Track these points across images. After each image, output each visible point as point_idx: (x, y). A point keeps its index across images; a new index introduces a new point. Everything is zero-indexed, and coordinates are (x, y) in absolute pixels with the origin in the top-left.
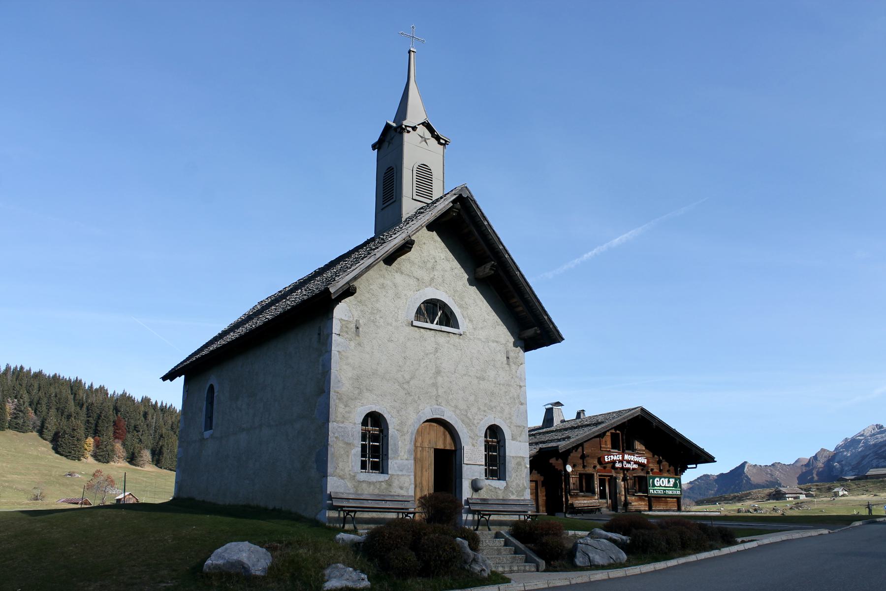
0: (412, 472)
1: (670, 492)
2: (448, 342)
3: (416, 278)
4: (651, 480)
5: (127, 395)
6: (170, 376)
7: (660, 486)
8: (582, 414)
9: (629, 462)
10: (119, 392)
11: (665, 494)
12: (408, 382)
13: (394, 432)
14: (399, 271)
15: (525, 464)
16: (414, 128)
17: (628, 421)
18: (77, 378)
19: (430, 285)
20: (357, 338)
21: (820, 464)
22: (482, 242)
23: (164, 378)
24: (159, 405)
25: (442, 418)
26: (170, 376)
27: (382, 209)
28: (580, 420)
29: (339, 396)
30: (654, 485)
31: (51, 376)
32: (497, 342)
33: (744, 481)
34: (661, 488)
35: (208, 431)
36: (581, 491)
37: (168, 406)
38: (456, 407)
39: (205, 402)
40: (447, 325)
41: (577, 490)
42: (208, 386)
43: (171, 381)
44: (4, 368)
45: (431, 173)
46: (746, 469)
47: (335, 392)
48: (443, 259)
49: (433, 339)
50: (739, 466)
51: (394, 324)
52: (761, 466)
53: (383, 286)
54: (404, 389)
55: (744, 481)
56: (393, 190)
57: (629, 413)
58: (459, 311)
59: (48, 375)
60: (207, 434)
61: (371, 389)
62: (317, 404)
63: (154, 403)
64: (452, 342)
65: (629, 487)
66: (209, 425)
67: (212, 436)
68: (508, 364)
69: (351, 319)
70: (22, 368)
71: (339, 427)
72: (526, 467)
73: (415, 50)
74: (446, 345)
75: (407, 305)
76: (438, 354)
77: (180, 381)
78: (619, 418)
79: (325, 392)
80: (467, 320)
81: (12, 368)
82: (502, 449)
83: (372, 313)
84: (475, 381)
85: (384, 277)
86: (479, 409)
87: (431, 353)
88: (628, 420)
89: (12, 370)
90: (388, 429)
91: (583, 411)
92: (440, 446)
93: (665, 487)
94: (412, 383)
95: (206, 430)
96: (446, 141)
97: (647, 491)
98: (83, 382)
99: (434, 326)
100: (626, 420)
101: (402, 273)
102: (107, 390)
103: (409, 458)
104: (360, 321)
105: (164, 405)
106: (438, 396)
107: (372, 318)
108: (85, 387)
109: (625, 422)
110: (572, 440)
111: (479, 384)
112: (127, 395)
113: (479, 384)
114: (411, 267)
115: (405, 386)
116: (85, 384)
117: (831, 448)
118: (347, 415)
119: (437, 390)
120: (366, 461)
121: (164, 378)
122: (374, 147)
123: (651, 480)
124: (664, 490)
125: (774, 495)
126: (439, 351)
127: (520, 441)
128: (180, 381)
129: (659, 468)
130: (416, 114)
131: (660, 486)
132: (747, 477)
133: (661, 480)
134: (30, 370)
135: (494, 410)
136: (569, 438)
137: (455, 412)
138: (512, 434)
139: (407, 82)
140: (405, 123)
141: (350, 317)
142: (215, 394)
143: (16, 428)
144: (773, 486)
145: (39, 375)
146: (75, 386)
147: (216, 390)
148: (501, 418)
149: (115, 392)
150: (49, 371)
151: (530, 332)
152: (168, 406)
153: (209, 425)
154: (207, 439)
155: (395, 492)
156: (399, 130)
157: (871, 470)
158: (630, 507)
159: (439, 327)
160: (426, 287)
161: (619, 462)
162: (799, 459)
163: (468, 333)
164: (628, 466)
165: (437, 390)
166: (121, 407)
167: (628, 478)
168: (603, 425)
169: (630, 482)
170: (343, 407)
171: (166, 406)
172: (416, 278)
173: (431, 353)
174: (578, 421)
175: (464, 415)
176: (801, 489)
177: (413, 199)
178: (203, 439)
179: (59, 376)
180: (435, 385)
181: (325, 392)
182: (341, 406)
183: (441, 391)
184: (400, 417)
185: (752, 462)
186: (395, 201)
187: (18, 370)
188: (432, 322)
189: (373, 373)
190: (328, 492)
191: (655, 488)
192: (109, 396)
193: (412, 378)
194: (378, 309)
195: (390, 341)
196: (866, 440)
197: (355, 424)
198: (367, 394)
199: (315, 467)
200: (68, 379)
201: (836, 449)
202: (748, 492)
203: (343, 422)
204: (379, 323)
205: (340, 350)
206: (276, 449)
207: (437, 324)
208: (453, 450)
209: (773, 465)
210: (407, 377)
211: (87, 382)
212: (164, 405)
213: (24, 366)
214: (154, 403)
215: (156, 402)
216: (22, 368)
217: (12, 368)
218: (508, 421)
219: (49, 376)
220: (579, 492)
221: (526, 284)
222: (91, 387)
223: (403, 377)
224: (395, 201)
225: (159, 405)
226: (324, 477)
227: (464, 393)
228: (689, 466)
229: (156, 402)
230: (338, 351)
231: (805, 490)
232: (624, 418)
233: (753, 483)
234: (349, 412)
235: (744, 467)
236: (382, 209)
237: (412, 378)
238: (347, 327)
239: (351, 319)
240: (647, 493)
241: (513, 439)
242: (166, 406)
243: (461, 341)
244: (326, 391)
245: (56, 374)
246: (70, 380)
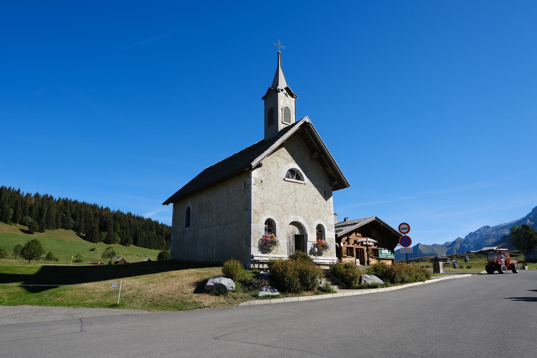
1: (389, 256)
4: (380, 251)
5: (120, 211)
6: (167, 203)
7: (384, 253)
8: (347, 219)
9: (369, 242)
10: (116, 210)
11: (387, 257)
12: (284, 205)
14: (279, 156)
15: (333, 241)
16: (282, 90)
17: (370, 223)
18: (95, 203)
20: (262, 186)
21: (458, 246)
22: (314, 142)
23: (164, 204)
24: (136, 216)
25: (298, 221)
26: (167, 203)
27: (268, 127)
28: (346, 222)
29: (255, 212)
30: (381, 253)
31: (82, 202)
32: (320, 187)
33: (419, 253)
34: (385, 254)
35: (187, 228)
36: (348, 255)
37: (140, 217)
38: (304, 216)
39: (185, 215)
40: (299, 180)
41: (346, 254)
42: (187, 207)
43: (167, 205)
44: (58, 199)
46: (420, 247)
47: (253, 210)
49: (293, 186)
50: (416, 245)
51: (277, 179)
52: (427, 245)
53: (272, 163)
54: (282, 208)
55: (419, 253)
57: (370, 219)
59: (80, 202)
60: (187, 229)
61: (268, 208)
62: (245, 215)
63: (133, 215)
64: (302, 187)
65: (370, 254)
66: (188, 224)
67: (190, 230)
69: (259, 177)
70: (67, 199)
71: (256, 225)
73: (280, 52)
74: (299, 188)
76: (296, 193)
77: (171, 205)
78: (365, 221)
81: (62, 199)
82: (323, 235)
83: (268, 175)
84: (312, 205)
85: (272, 159)
86: (314, 217)
87: (293, 192)
88: (369, 222)
89: (62, 200)
90: (275, 226)
91: (347, 218)
92: (297, 233)
93: (387, 254)
94: (285, 206)
95: (186, 227)
96: (296, 96)
97: (378, 256)
98: (98, 205)
99: (294, 180)
100: (368, 222)
101: (280, 157)
102: (110, 209)
105: (139, 216)
106: (296, 211)
108: (99, 208)
109: (368, 223)
110: (344, 231)
111: (314, 206)
112: (120, 211)
113: (314, 206)
114: (284, 154)
115: (283, 207)
116: (99, 206)
117: (463, 237)
118: (258, 220)
119: (296, 209)
121: (164, 204)
122: (263, 98)
123: (380, 251)
124: (387, 255)
125: (434, 260)
127: (331, 232)
128: (171, 205)
130: (282, 84)
131: (384, 253)
132: (420, 250)
133: (385, 251)
134: (71, 200)
135: (320, 217)
136: (342, 230)
137: (303, 218)
138: (328, 228)
139: (278, 67)
140: (278, 87)
142: (191, 211)
143: (64, 228)
144: (434, 255)
145: (75, 202)
146: (95, 207)
147: (191, 209)
148: (323, 221)
149: (114, 210)
150: (81, 200)
151: (336, 183)
152: (140, 217)
153: (188, 224)
154: (187, 231)
156: (275, 91)
157: (484, 248)
158: (370, 263)
161: (365, 242)
162: (446, 242)
164: (369, 244)
165: (296, 209)
166: (117, 217)
167: (369, 249)
168: (358, 225)
169: (370, 251)
170: (257, 216)
171: (139, 217)
173: (293, 192)
174: (345, 222)
175: (307, 220)
176: (448, 257)
177: (282, 123)
178: (185, 231)
179: (86, 203)
180: (295, 206)
182: (256, 216)
183: (297, 209)
184: (280, 221)
185: (423, 243)
187: (49, 197)
189: (269, 202)
190: (252, 254)
191: (382, 254)
192: (111, 212)
193: (285, 203)
194: (270, 173)
195: (276, 187)
196: (481, 234)
197: (262, 224)
198: (267, 211)
200: (90, 204)
201: (466, 237)
202: (421, 257)
203: (257, 223)
205: (255, 191)
207: (295, 179)
208: (299, 235)
209: (433, 245)
210: (283, 203)
211: (100, 205)
212: (139, 216)
213: (68, 198)
214: (133, 215)
215: (135, 215)
216: (67, 199)
217: (62, 199)
218: (326, 222)
219: (81, 203)
220: (346, 255)
222: (102, 208)
223: (282, 203)
225: (136, 216)
226: (249, 247)
227: (307, 210)
228: (398, 244)
229: (135, 215)
231: (450, 257)
232: (367, 221)
233: (423, 253)
234: (259, 219)
235: (419, 246)
236: (268, 127)
237: (285, 203)
240: (378, 257)
241: (328, 230)
242: (139, 217)
244: (249, 209)
245: (84, 202)
246: (91, 205)
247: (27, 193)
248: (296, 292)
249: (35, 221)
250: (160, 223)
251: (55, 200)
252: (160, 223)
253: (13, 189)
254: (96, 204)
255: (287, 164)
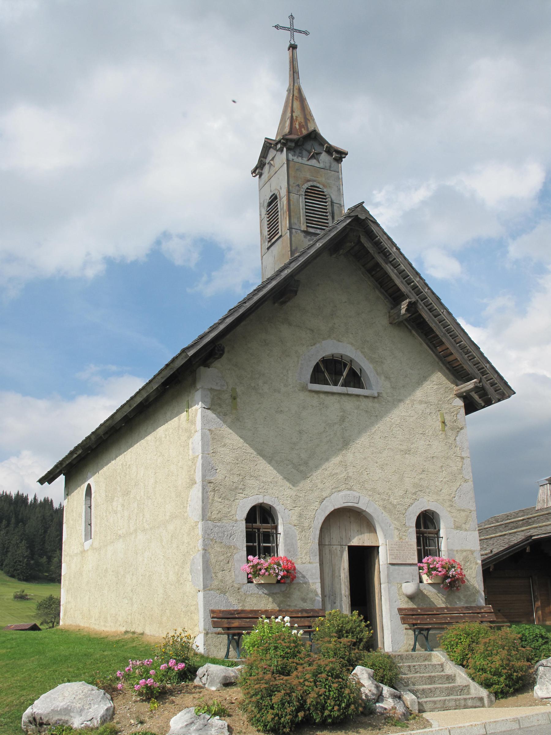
0: (317, 578)
2: (358, 408)
3: (309, 329)
13: (290, 528)
19: (329, 336)
20: (234, 411)
25: (356, 505)
27: (268, 249)
43: (49, 483)
45: (325, 196)
48: (345, 302)
56: (278, 222)
58: (371, 366)
62: (189, 499)
66: (88, 535)
68: (443, 430)
72: (477, 564)
74: (356, 411)
75: (299, 365)
79: (196, 483)
80: (383, 378)
87: (335, 423)
95: (86, 540)
99: (338, 389)
103: (312, 561)
104: (237, 390)
107: (253, 385)
120: (421, 549)
126: (347, 420)
129: (240, 639)
141: (224, 385)
153: (88, 535)
154: (88, 550)
155: (296, 606)
159: (344, 390)
160: (324, 339)
163: (384, 395)
172: (309, 329)
173: (335, 423)
178: (84, 550)
181: (196, 483)
186: (281, 236)
188: (336, 384)
199: (190, 579)
204: (262, 390)
206: (151, 559)
210: (304, 456)
221: (294, 263)
224: (281, 236)
230: (209, 430)
236: (268, 249)
238: (220, 398)
239: (225, 388)
243: (377, 405)
247: (16, 493)
248: (196, 611)
249: (488, 551)
250: (13, 495)
251: (41, 501)
252: (13, 495)
253: (35, 499)
254: (20, 493)
255: (314, 344)
